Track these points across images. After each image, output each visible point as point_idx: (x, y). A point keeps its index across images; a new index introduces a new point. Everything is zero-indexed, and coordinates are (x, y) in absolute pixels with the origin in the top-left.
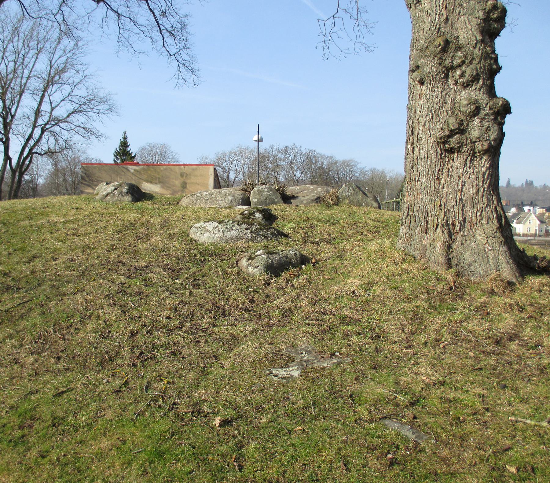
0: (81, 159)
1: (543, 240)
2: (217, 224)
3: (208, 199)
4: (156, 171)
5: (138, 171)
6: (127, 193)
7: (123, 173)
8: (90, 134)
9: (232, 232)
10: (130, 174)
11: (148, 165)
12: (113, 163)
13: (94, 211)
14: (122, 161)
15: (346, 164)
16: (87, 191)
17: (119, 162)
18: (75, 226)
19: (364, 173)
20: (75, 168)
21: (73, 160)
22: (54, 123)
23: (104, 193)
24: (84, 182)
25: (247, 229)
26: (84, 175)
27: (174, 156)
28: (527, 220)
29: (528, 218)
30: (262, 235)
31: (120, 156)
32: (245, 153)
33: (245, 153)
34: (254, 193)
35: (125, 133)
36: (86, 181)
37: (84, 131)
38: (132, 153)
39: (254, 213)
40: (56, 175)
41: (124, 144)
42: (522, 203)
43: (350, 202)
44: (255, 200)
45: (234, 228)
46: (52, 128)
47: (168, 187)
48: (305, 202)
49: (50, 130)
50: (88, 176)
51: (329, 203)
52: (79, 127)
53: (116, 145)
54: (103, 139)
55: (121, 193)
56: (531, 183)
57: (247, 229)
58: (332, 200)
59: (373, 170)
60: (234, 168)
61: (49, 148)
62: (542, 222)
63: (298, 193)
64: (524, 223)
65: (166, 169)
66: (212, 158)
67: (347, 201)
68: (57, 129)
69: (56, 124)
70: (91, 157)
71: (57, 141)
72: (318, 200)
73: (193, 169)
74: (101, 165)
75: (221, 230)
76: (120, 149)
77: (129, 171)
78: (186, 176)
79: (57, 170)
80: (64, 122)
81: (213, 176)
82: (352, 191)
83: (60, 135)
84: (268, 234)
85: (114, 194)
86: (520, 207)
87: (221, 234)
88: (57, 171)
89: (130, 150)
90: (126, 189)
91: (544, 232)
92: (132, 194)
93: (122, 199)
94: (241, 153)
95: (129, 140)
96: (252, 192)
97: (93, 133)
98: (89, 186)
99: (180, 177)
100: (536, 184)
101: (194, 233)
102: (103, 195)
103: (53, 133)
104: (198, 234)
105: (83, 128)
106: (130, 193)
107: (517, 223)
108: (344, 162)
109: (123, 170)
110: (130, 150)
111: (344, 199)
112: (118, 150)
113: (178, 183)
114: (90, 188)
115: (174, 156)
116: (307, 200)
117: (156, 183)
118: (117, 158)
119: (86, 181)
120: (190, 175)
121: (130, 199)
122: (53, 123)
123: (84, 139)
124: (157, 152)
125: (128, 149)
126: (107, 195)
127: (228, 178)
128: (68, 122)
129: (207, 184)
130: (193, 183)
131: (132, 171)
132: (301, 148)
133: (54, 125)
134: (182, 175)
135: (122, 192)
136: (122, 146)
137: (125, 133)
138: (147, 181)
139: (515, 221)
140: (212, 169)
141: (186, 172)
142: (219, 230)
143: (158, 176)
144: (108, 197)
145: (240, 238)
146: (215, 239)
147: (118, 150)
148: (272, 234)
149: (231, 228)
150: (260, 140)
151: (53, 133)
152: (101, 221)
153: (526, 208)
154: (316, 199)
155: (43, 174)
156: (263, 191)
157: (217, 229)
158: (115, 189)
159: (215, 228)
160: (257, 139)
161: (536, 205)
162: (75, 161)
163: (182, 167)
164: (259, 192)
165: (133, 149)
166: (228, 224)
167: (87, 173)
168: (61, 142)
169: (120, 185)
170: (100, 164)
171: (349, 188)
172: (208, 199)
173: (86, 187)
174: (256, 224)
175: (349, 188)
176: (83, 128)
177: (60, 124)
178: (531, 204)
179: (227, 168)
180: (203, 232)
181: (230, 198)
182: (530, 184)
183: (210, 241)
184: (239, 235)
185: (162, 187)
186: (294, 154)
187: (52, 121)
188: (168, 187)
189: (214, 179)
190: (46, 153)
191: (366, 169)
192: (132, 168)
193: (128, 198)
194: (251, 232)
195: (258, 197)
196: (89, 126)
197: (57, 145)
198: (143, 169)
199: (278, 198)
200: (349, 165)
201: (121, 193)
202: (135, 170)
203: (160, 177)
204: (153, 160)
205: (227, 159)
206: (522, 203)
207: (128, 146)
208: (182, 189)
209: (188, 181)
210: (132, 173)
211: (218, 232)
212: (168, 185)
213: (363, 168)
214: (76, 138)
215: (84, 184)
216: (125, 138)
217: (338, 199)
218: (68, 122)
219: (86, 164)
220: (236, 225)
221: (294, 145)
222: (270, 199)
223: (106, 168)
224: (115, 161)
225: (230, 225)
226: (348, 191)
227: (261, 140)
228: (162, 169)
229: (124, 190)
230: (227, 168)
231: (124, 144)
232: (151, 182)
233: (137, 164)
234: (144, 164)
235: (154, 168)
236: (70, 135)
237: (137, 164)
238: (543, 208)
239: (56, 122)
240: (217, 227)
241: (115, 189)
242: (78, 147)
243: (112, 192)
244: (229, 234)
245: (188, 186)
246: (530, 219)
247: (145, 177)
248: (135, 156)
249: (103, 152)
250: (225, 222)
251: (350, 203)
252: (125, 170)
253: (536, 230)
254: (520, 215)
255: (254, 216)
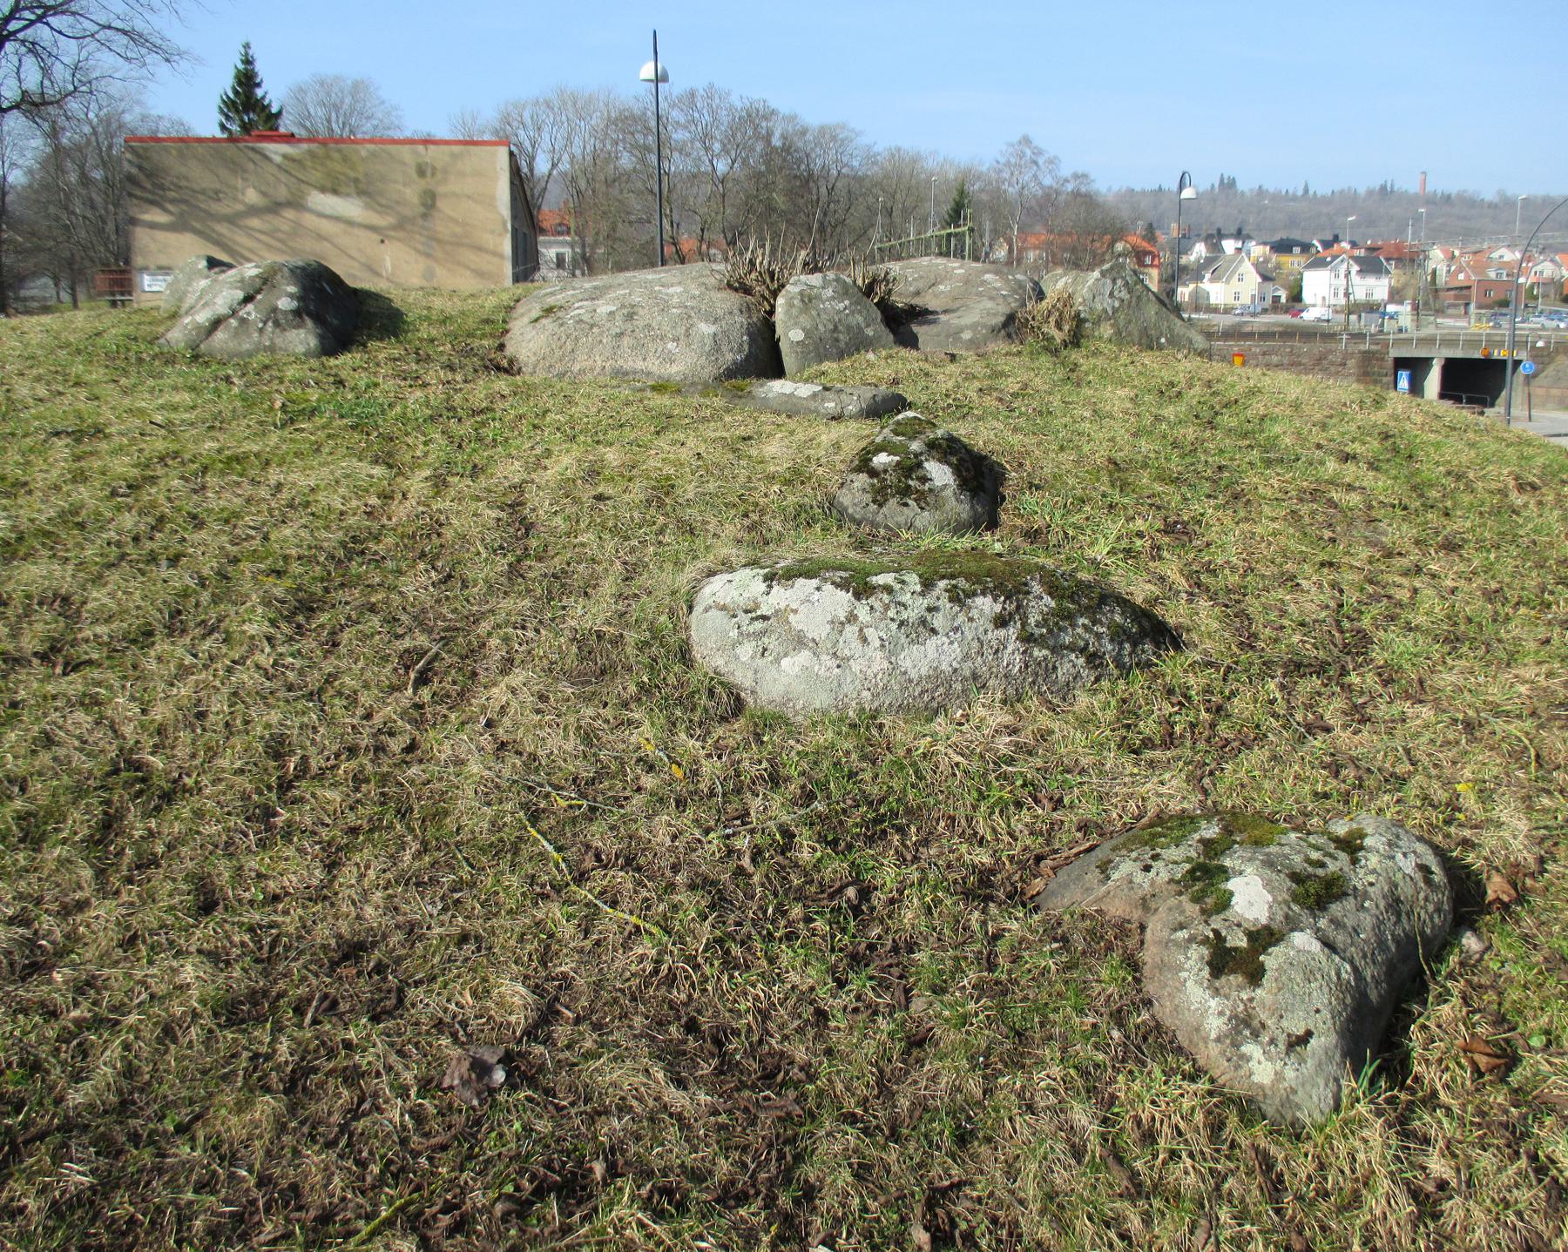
0: (127, 118)
1: (1274, 324)
2: (845, 597)
3: (620, 335)
4: (345, 159)
5: (293, 160)
6: (297, 313)
7: (251, 166)
8: (144, 51)
9: (932, 643)
10: (274, 170)
11: (324, 143)
12: (219, 134)
13: (160, 446)
14: (246, 128)
15: (830, 136)
16: (147, 217)
17: (235, 128)
18: (63, 577)
19: (871, 158)
20: (110, 147)
21: (107, 121)
22: (33, 17)
23: (203, 317)
24: (138, 193)
25: (1001, 622)
26: (134, 171)
27: (389, 114)
28: (1234, 272)
29: (1237, 268)
30: (1072, 648)
31: (237, 111)
32: (575, 104)
33: (575, 104)
34: (790, 305)
35: (247, 46)
36: (144, 189)
37: (124, 40)
38: (269, 105)
39: (919, 465)
40: (60, 168)
41: (247, 79)
42: (1219, 231)
43: (1118, 333)
44: (797, 335)
45: (938, 621)
46: (29, 31)
47: (387, 207)
48: (967, 335)
49: (20, 36)
50: (149, 176)
51: (1050, 339)
52: (109, 27)
53: (224, 83)
54: (184, 65)
55: (273, 315)
56: (1232, 183)
57: (1001, 622)
58: (1059, 326)
59: (896, 153)
60: (545, 143)
61: (24, 93)
62: (1266, 278)
63: (918, 293)
64: (1227, 282)
65: (373, 154)
66: (487, 116)
67: (1107, 331)
68: (41, 33)
69: (40, 19)
70: (154, 112)
71: (46, 72)
72: (1011, 330)
73: (454, 156)
74: (187, 143)
75: (870, 633)
76: (236, 93)
77: (266, 158)
78: (433, 174)
79: (58, 150)
80: (63, 13)
81: (507, 175)
82: (1124, 295)
83: (55, 52)
84: (1098, 636)
85: (243, 321)
86: (1215, 240)
87: (879, 663)
88: (58, 156)
89: (263, 98)
90: (291, 296)
91: (1269, 301)
92: (318, 319)
93: (279, 341)
94: (572, 106)
95: (262, 69)
96: (780, 301)
97: (155, 48)
98: (153, 203)
99: (415, 176)
100: (1243, 185)
101: (717, 644)
102: (198, 327)
103: (33, 48)
104: (746, 651)
105: (125, 32)
106: (310, 315)
107: (1212, 280)
108: (822, 130)
109: (252, 155)
110: (263, 98)
111: (1097, 323)
112: (232, 96)
113: (412, 195)
114: (158, 210)
115: (389, 114)
116: (974, 327)
117: (348, 195)
118: (228, 117)
119: (144, 189)
120: (445, 171)
121: (313, 342)
122: (27, 15)
123: (127, 66)
124: (342, 102)
125: (259, 92)
126: (217, 323)
127: (531, 170)
128: (73, 14)
129: (493, 198)
130: (454, 195)
131: (278, 159)
132: (728, 94)
133: (32, 23)
134: (421, 172)
135: (275, 310)
136: (240, 83)
137: (247, 46)
138: (323, 190)
139: (1208, 276)
140: (502, 154)
141: (430, 160)
142: (864, 640)
143: (352, 174)
144: (220, 335)
145: (975, 676)
146: (848, 688)
147: (232, 96)
148: (1118, 635)
149: (923, 622)
150: (660, 78)
151: (33, 48)
152: (197, 522)
153: (1229, 246)
154: (1005, 325)
155: (20, 162)
156: (818, 297)
157: (851, 631)
158: (248, 299)
159: (839, 626)
160: (653, 77)
161: (1249, 237)
162: (111, 124)
163: (421, 148)
164: (808, 300)
165: (273, 91)
166: (906, 598)
167: (145, 165)
168: (60, 73)
169: (266, 281)
170: (182, 140)
171: (1114, 281)
172: (620, 335)
173: (146, 206)
174: (1037, 588)
175: (1114, 281)
176: (125, 32)
177: (54, 21)
178: (1239, 235)
179: (527, 144)
180: (770, 641)
181: (706, 329)
182: (1228, 185)
183: (822, 700)
184: (966, 657)
185: (368, 206)
186: (713, 112)
187: (26, 8)
188: (387, 207)
189: (512, 183)
190: (17, 106)
191: (876, 149)
192: (276, 150)
193: (303, 338)
194: (1027, 639)
195: (805, 321)
196: (139, 25)
197: (47, 83)
198: (311, 153)
199: (875, 328)
200: (834, 138)
201: (273, 315)
202: (285, 156)
203: (360, 177)
204: (329, 121)
205: (528, 121)
206: (1219, 231)
207: (259, 85)
208: (422, 210)
209: (441, 190)
210: (279, 166)
211: (856, 644)
212: (384, 202)
213: (869, 148)
214: (104, 61)
215: (137, 197)
216: (248, 61)
217: (1079, 321)
218: (73, 14)
219: (141, 140)
220: (944, 603)
221: (711, 86)
222: (849, 328)
223: (200, 149)
224: (223, 127)
225: (916, 607)
226: (1111, 295)
227: (665, 79)
228: (364, 153)
229: (285, 304)
230: (527, 144)
231: (247, 79)
232: (335, 192)
233: (290, 138)
234: (309, 140)
235: (339, 151)
236: (84, 54)
237: (290, 138)
238: (1265, 244)
239: (39, 12)
240: (852, 618)
241: (248, 299)
242: (115, 88)
243: (234, 313)
244: (922, 658)
245: (439, 204)
246: (1241, 270)
247: (316, 176)
248: (280, 113)
249: (190, 104)
250: (888, 589)
251: (1120, 338)
252: (257, 157)
253: (1253, 297)
254: (1213, 265)
255: (924, 479)
